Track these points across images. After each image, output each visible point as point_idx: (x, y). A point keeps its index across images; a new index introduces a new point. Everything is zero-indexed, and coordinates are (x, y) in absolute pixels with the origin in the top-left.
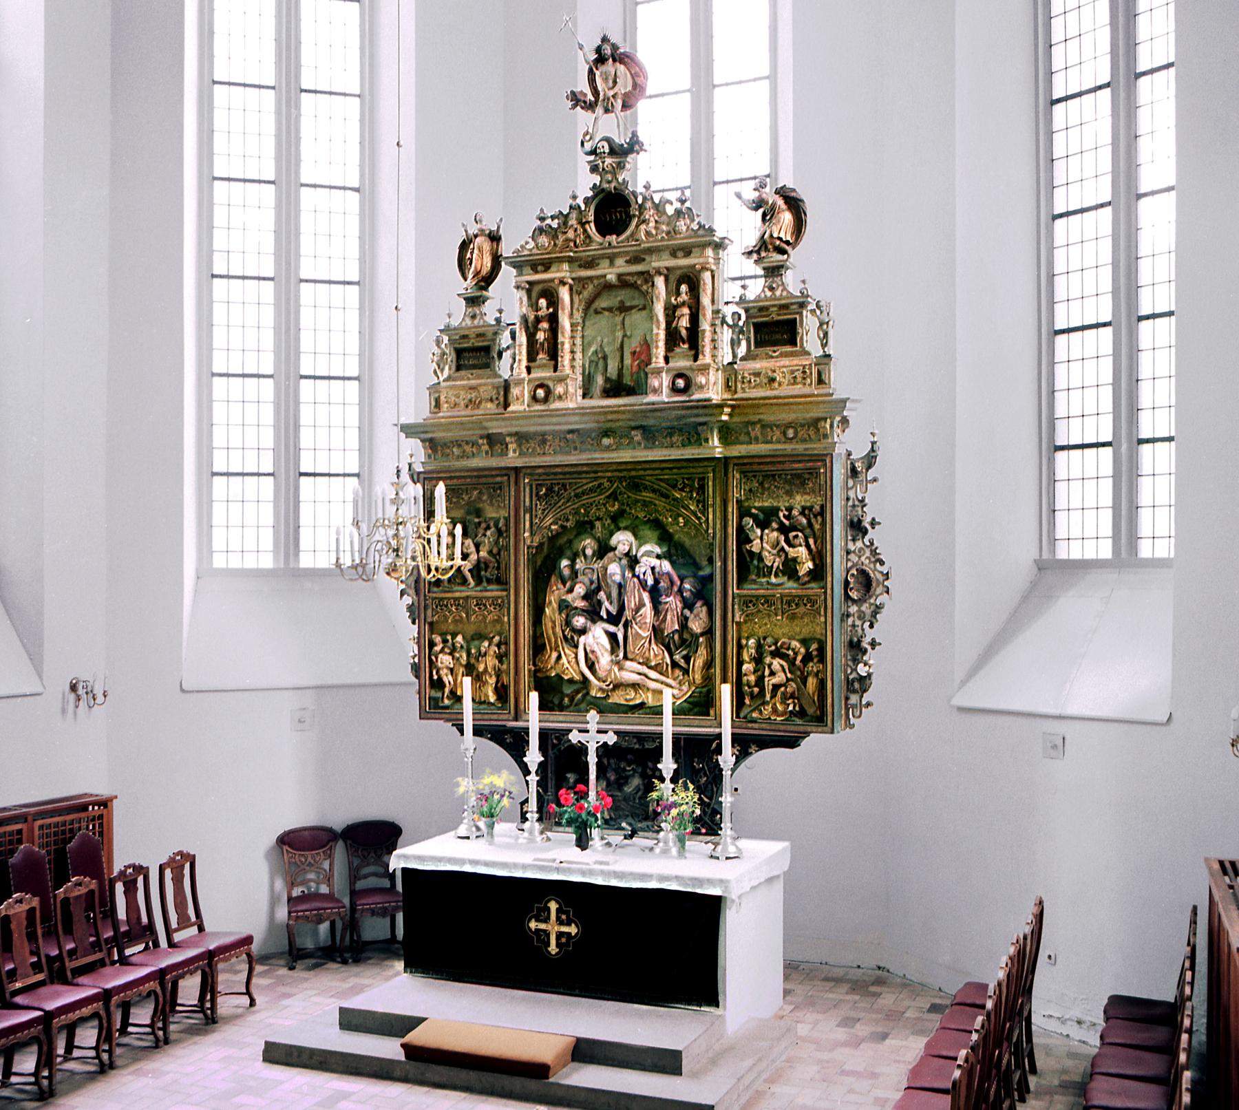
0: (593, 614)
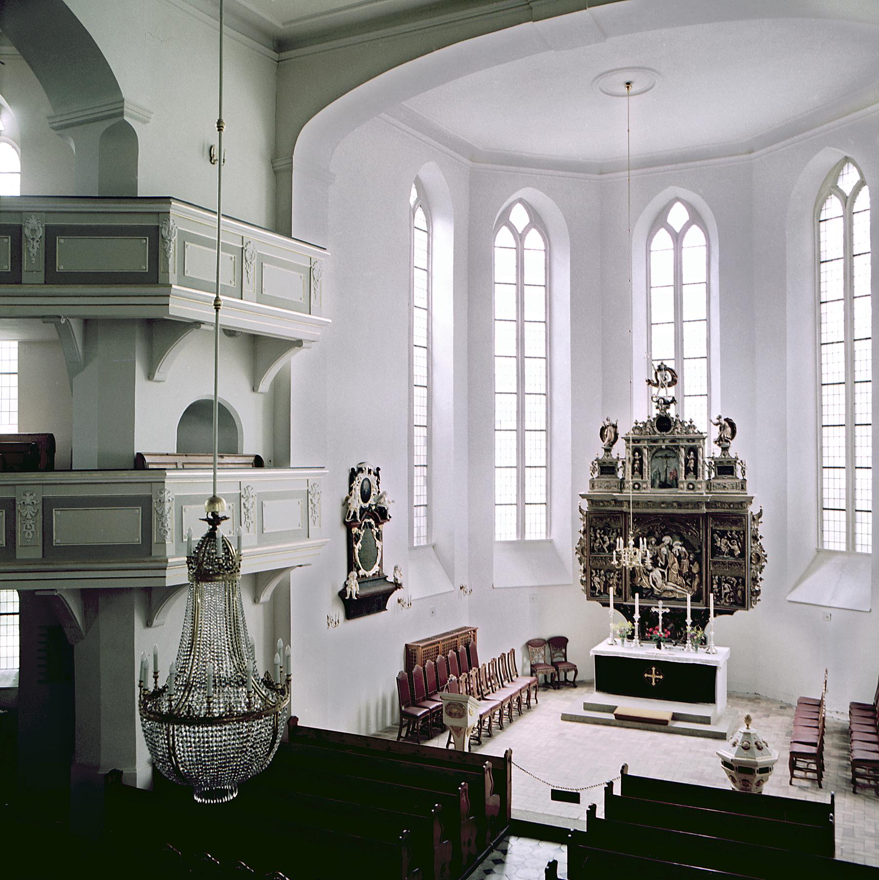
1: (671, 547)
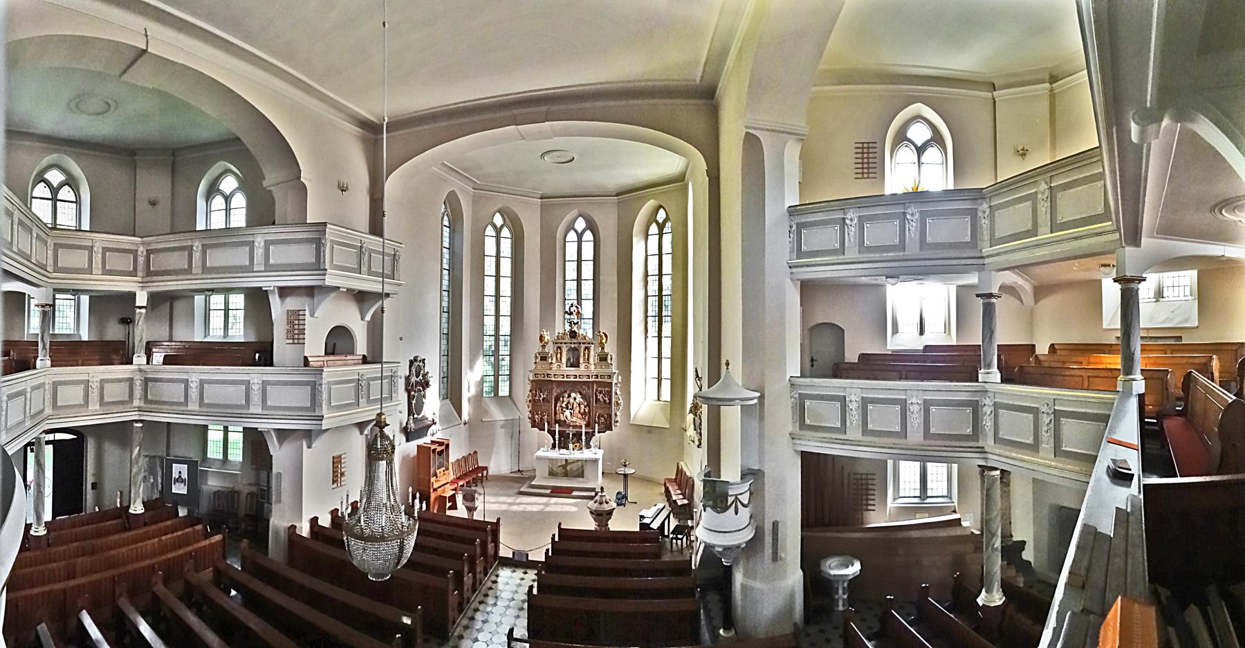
0: (567, 409)
1: (575, 399)
